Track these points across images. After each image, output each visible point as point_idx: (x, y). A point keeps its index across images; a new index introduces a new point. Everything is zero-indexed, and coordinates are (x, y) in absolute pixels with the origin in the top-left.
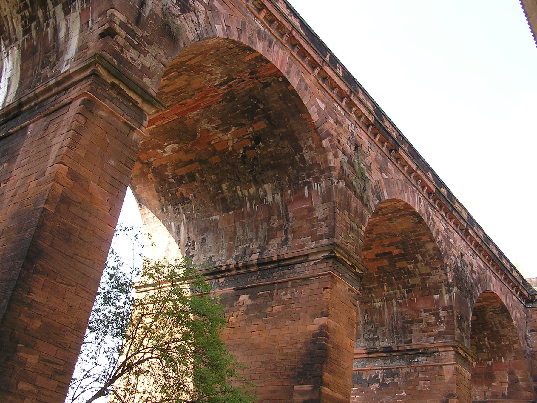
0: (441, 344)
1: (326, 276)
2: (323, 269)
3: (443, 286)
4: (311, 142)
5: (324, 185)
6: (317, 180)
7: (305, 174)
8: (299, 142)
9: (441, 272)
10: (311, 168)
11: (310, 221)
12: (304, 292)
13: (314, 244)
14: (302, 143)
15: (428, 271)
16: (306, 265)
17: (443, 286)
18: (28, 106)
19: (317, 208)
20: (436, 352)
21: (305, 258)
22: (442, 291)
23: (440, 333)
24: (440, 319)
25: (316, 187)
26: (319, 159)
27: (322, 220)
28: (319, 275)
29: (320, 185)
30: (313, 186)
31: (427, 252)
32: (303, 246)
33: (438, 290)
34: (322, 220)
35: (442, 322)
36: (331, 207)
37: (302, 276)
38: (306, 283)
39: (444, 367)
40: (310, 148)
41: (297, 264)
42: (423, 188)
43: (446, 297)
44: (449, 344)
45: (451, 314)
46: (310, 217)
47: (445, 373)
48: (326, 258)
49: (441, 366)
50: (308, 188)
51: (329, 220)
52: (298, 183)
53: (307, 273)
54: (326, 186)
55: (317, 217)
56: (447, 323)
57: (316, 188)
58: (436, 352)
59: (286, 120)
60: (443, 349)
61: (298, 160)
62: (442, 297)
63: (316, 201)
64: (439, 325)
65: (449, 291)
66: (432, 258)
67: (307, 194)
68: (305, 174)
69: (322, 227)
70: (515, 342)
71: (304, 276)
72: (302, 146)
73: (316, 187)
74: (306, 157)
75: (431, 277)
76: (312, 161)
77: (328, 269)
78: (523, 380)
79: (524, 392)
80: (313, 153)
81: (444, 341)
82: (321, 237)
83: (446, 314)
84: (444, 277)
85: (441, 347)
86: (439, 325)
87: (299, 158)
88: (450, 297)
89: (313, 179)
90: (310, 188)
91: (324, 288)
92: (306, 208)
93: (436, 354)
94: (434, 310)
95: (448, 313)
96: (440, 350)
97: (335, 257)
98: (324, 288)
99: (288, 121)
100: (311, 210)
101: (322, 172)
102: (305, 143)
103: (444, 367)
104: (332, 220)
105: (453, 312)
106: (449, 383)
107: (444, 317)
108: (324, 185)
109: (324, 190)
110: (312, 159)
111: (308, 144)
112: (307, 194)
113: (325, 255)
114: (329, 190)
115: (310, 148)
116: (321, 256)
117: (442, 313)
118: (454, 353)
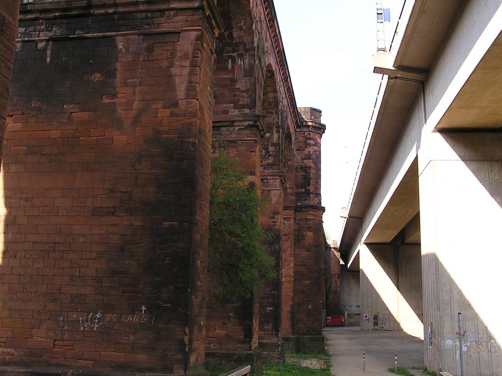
0: (271, 174)
1: (252, 142)
2: (248, 136)
3: (275, 127)
4: (242, 24)
5: (247, 61)
6: (241, 56)
7: (231, 48)
8: (231, 21)
9: (275, 116)
10: (237, 45)
11: (233, 90)
12: (232, 152)
13: (236, 112)
14: (234, 23)
15: (265, 114)
16: (231, 129)
17: (275, 127)
18: (103, 11)
19: (238, 80)
20: (265, 179)
21: (230, 124)
22: (272, 131)
23: (268, 164)
24: (269, 153)
25: (239, 62)
26: (246, 39)
27: (243, 92)
28: (245, 140)
29: (243, 61)
30: (237, 60)
31: (267, 99)
32: (226, 112)
33: (270, 130)
34: (243, 92)
35: (270, 155)
36: (253, 82)
37: (228, 138)
38: (232, 144)
39: (272, 191)
40: (241, 29)
41: (222, 127)
42: (276, 48)
43: (275, 136)
44: (277, 174)
45: (278, 150)
46: (232, 86)
47: (272, 196)
48: (249, 126)
49: (269, 191)
50: (232, 62)
51: (250, 93)
52: (222, 56)
53: (233, 136)
54: (249, 63)
55: (239, 88)
56: (275, 157)
57: (239, 63)
58: (265, 179)
59: (226, 2)
60: (271, 178)
61: (226, 35)
62: (272, 135)
63: (238, 74)
64: (268, 157)
65: (278, 132)
66: (270, 105)
67: (230, 66)
68: (231, 48)
69: (243, 97)
70: (290, 160)
71: (230, 139)
72: (234, 25)
73: (239, 62)
74: (235, 35)
75: (265, 119)
76: (239, 40)
77: (252, 135)
78: (290, 188)
79: (290, 196)
80: (242, 33)
81: (271, 171)
82: (243, 106)
83: (274, 150)
84: (276, 120)
85: (270, 176)
86: (268, 157)
87: (227, 34)
88: (279, 136)
89: (238, 55)
90: (234, 62)
91: (250, 152)
92: (229, 78)
93: (265, 181)
94: (264, 145)
95: (276, 149)
96: (269, 178)
97: (257, 127)
98: (250, 152)
99: (228, 2)
100: (233, 81)
101: (247, 50)
102: (237, 24)
103: (272, 191)
104: (253, 93)
105: (279, 148)
106: (275, 204)
107: (272, 151)
108: (247, 61)
109: (247, 66)
110: (240, 38)
111: (239, 25)
112: (230, 66)
113: (250, 123)
114: (252, 67)
115: (241, 29)
116: (246, 123)
117: (271, 148)
118: (280, 180)
